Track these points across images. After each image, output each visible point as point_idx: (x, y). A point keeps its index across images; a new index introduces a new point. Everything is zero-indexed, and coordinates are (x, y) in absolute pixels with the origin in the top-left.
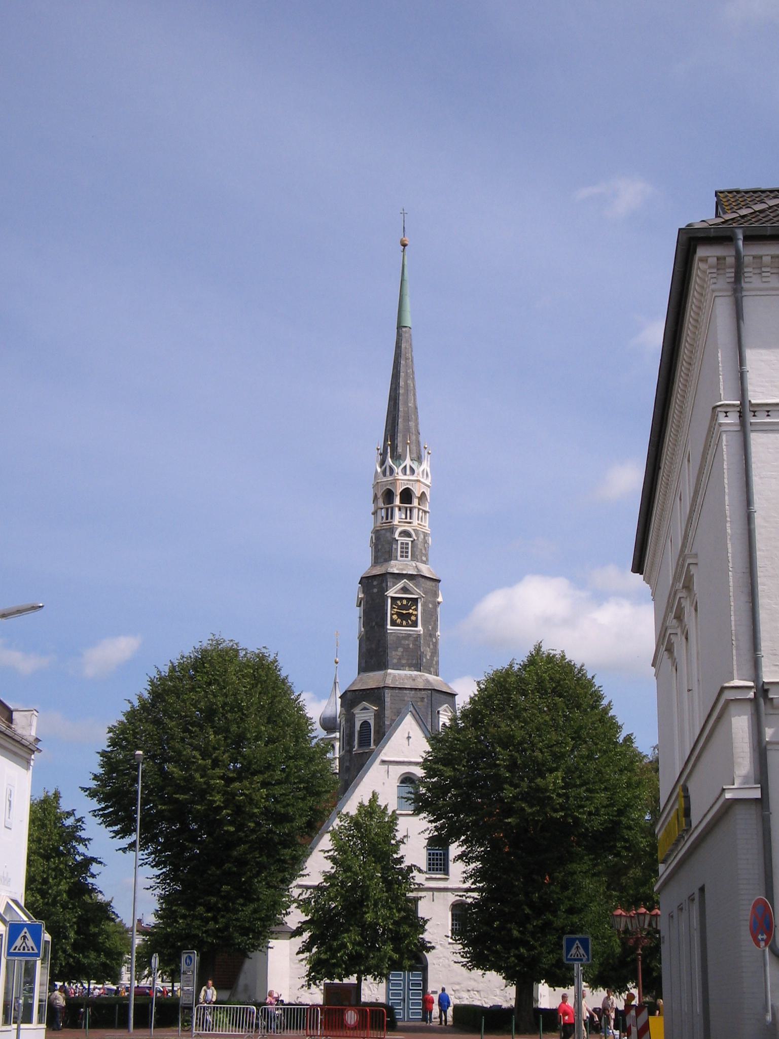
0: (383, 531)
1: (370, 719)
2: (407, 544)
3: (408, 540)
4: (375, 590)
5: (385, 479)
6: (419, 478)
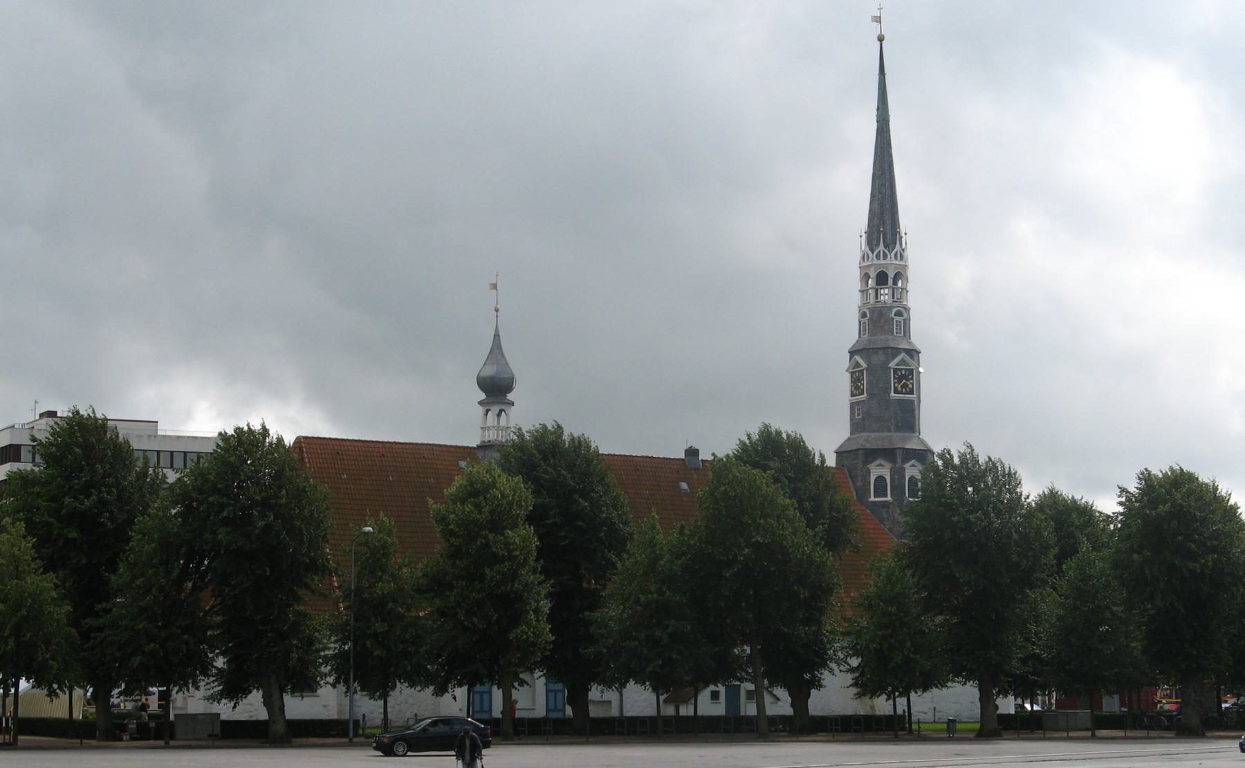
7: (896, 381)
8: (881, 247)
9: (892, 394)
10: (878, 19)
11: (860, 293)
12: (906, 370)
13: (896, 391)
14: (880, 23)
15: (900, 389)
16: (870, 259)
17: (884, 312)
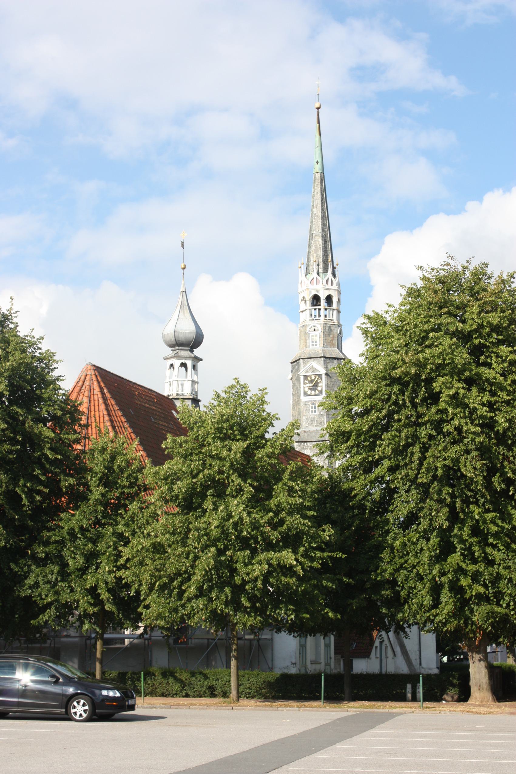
17: (332, 328)
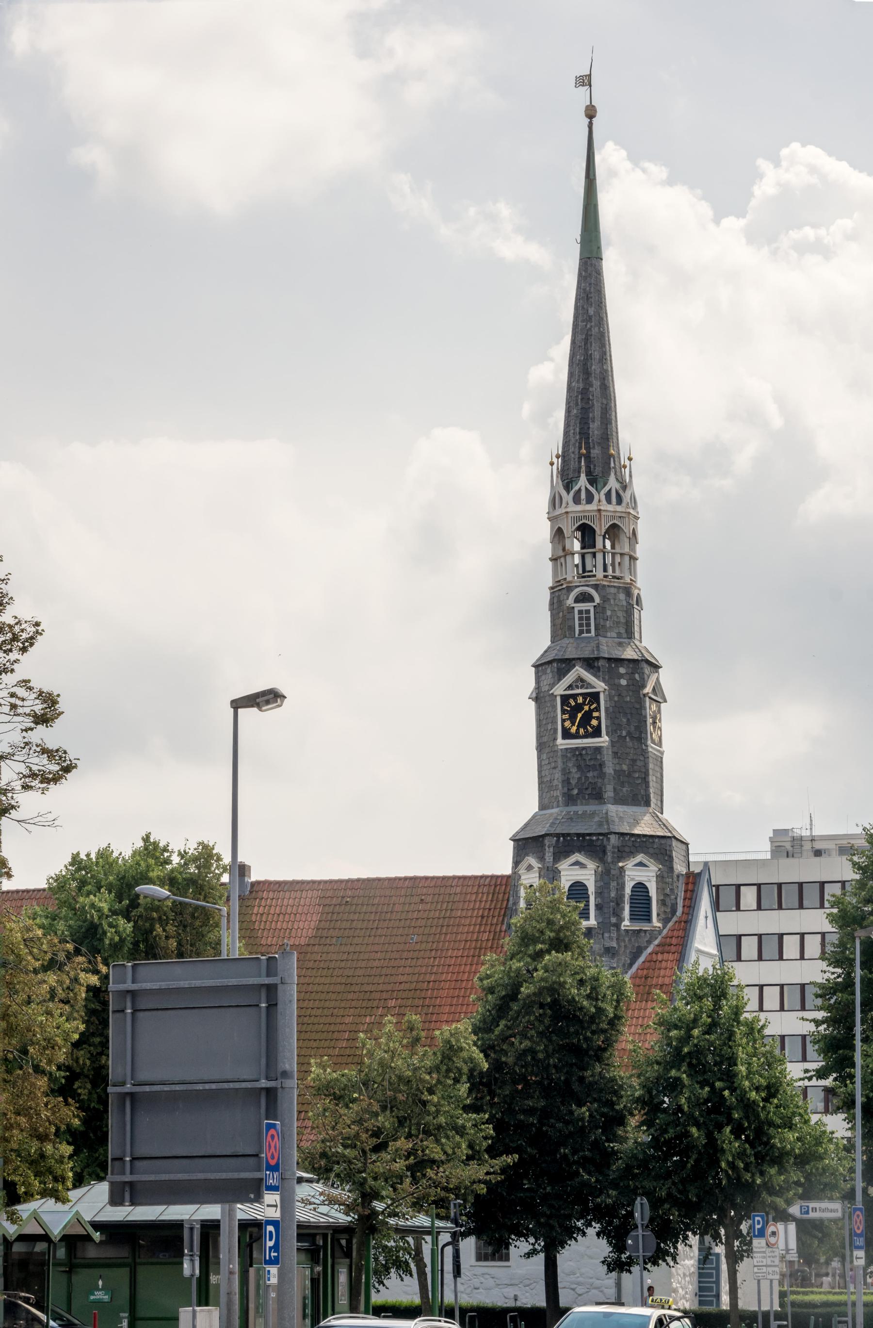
0: (613, 590)
1: (649, 881)
2: (588, 612)
3: (588, 606)
4: (624, 682)
5: (579, 508)
6: (628, 510)
7: (595, 714)
8: (583, 481)
9: (560, 741)
10: (585, 81)
11: (550, 563)
12: (584, 695)
13: (567, 734)
14: (590, 86)
15: (574, 730)
16: (564, 505)
